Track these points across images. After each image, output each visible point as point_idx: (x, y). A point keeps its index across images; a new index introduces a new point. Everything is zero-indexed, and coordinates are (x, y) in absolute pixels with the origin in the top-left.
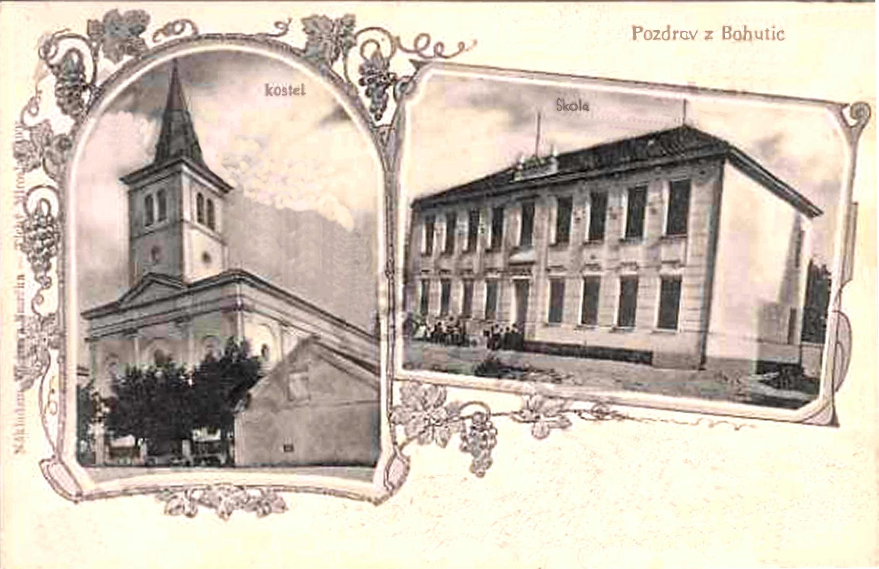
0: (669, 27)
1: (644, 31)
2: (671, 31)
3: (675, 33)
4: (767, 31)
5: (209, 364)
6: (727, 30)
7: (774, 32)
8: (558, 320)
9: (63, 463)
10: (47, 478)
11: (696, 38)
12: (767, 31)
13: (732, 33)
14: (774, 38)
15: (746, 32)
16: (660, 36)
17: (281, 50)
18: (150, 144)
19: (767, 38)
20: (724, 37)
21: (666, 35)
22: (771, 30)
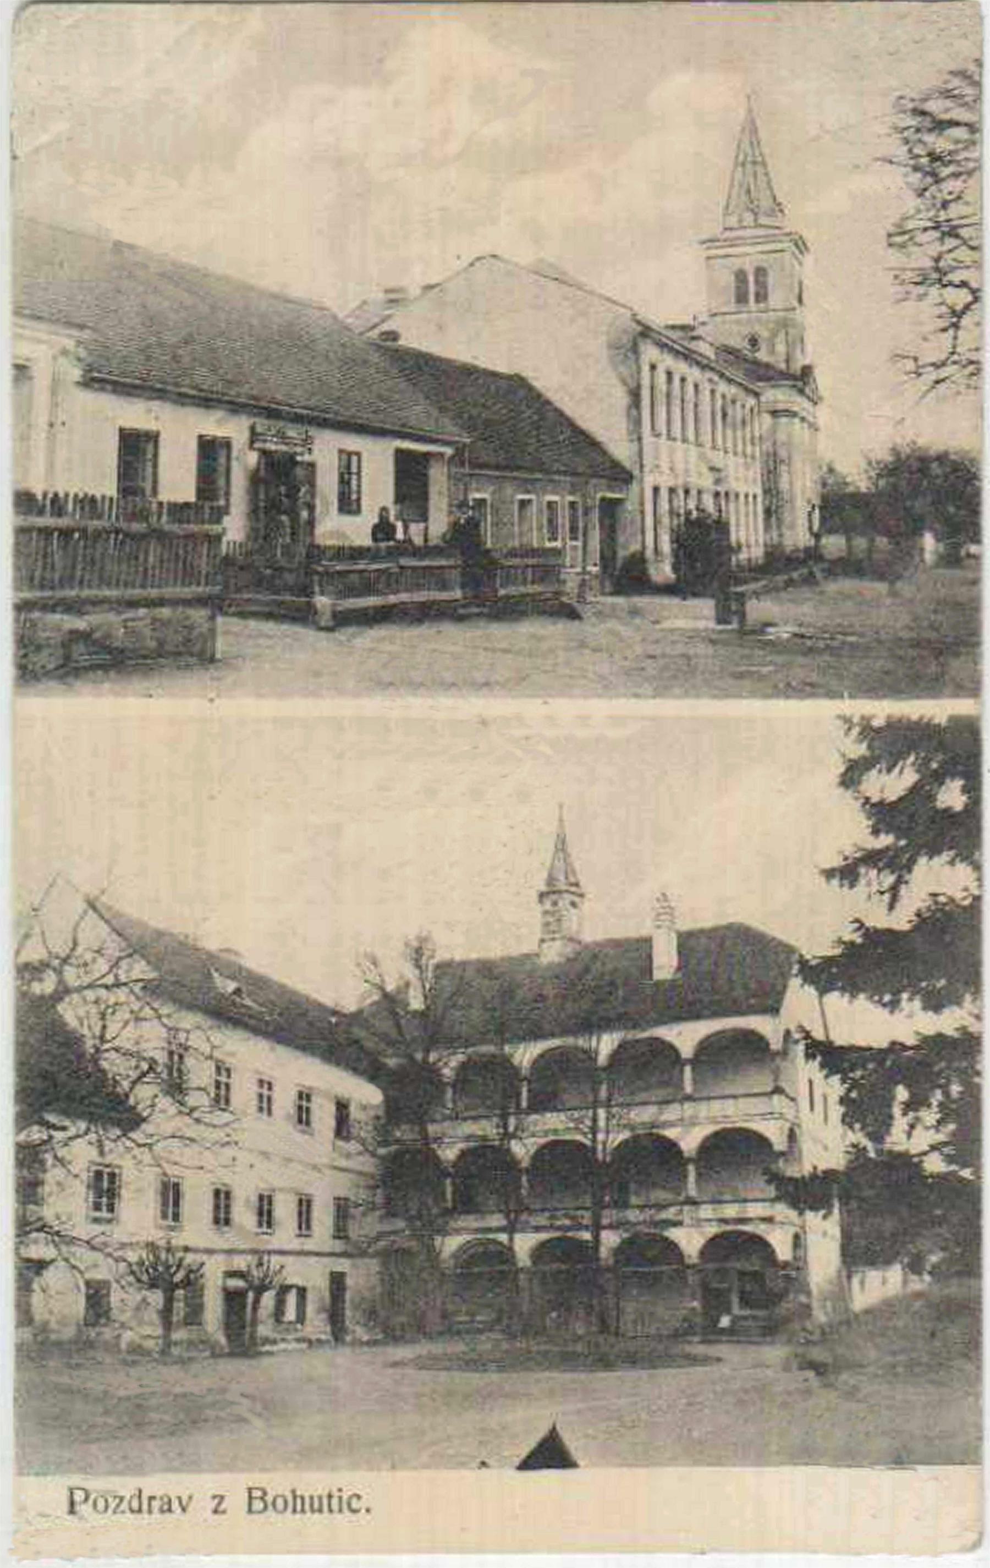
0: (140, 1491)
1: (92, 1497)
2: (145, 1496)
3: (151, 1498)
4: (330, 1496)
5: (463, 1154)
6: (257, 1494)
7: (340, 1498)
8: (973, 1458)
9: (954, 347)
10: (766, 174)
11: (190, 1509)
12: (330, 1496)
13: (269, 1499)
14: (340, 1511)
15: (295, 1497)
16: (124, 1506)
17: (19, 982)
18: (136, 694)
19: (331, 1511)
20: (250, 1511)
21: (135, 1505)
22: (336, 1494)
